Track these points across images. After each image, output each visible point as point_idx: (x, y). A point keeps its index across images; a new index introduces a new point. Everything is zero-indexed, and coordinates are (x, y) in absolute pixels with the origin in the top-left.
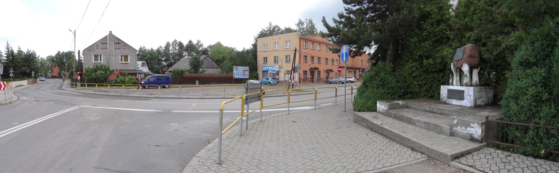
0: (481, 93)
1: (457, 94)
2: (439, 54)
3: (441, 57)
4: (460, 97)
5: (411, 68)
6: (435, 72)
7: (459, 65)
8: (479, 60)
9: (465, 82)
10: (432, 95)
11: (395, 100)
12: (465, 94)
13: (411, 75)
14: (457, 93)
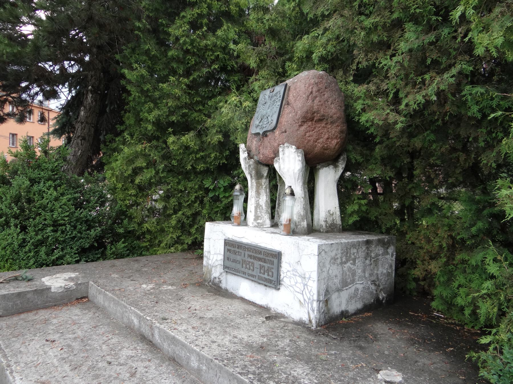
0: (349, 264)
1: (257, 264)
2: (214, 118)
3: (220, 127)
4: (266, 276)
5: (130, 161)
6: (206, 172)
7: (266, 152)
8: (341, 132)
9: (284, 217)
10: (196, 238)
11: (62, 264)
12: (285, 267)
13: (133, 182)
14: (255, 258)
